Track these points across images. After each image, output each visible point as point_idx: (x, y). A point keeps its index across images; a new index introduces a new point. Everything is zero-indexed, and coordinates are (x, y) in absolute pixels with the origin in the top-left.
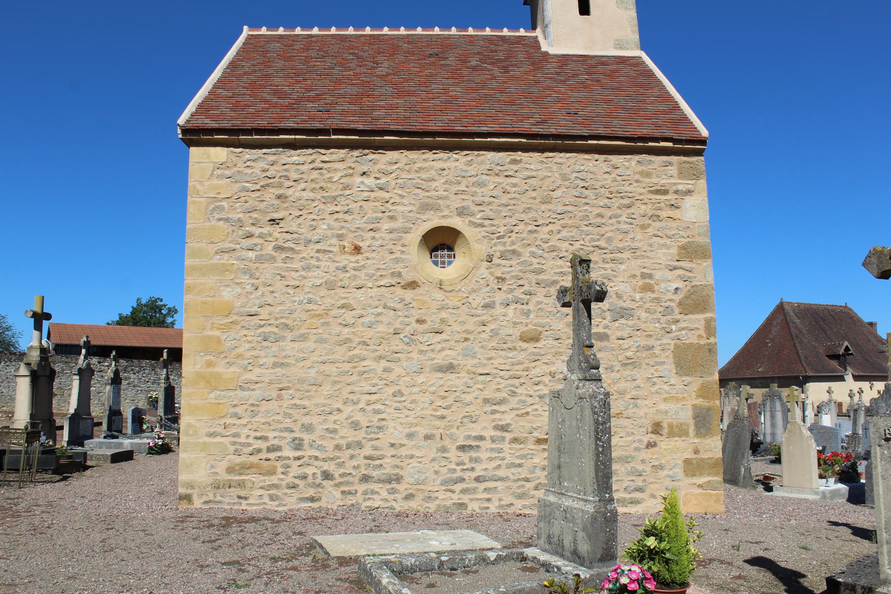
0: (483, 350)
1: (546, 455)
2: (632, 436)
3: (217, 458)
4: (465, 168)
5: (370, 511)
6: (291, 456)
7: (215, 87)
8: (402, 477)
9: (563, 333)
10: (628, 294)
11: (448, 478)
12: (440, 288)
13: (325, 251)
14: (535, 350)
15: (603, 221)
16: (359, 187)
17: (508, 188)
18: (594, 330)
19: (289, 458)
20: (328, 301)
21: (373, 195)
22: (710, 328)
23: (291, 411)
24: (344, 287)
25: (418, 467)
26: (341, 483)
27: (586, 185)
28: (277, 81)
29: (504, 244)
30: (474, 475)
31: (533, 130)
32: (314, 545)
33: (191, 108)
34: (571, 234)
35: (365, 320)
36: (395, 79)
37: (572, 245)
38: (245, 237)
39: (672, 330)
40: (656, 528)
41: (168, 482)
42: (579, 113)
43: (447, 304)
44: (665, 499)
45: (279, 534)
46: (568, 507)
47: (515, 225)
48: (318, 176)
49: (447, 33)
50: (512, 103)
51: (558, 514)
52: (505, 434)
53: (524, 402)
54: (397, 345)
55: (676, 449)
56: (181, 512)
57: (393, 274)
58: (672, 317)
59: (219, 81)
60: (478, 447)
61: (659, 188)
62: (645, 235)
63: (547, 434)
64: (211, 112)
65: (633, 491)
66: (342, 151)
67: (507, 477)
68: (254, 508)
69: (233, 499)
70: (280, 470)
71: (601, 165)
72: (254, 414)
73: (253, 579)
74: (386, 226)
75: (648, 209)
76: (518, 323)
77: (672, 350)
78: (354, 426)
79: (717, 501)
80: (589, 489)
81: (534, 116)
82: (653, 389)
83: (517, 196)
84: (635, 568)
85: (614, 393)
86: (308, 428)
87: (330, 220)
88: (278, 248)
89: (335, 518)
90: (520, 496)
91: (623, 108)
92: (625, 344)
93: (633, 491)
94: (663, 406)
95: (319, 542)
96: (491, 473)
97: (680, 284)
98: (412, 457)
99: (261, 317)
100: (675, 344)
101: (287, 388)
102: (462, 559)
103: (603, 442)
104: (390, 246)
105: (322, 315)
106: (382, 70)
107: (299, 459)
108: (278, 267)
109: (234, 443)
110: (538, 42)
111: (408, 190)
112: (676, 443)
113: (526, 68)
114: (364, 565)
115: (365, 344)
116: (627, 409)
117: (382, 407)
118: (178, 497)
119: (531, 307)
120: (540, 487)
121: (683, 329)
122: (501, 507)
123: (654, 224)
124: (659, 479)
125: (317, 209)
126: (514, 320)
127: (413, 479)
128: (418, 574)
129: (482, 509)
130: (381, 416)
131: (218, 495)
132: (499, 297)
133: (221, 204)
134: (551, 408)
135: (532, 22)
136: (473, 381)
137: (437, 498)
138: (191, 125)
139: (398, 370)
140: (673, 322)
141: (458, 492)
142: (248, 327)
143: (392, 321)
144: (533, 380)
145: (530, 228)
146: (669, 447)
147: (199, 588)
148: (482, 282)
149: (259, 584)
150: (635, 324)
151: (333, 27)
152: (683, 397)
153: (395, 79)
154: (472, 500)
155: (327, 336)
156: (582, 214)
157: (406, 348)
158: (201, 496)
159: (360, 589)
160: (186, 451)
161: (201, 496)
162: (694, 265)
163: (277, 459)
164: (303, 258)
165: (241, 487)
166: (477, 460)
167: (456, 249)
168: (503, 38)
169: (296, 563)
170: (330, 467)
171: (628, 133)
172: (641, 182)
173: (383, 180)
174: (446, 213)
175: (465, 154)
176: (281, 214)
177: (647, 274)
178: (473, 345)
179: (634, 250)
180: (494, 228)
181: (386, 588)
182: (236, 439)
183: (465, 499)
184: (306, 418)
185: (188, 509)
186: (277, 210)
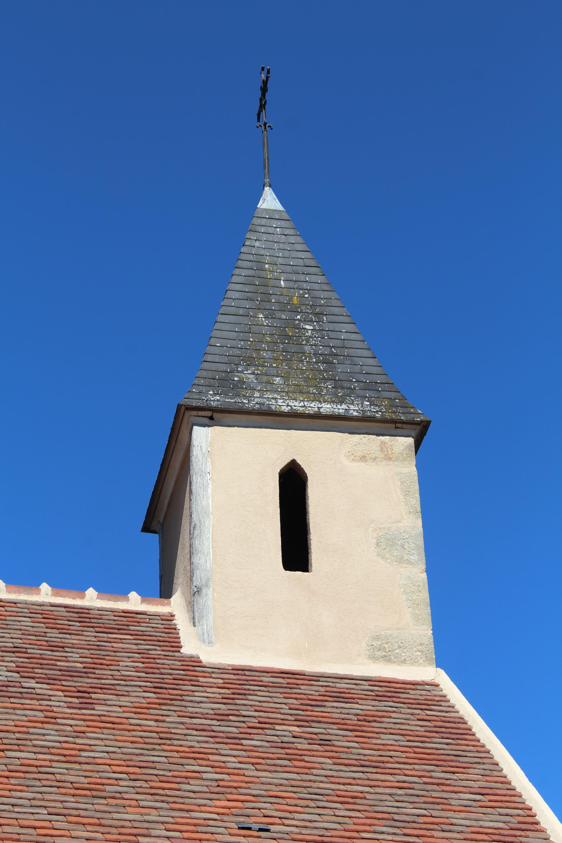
42: (272, 828)
135: (161, 577)
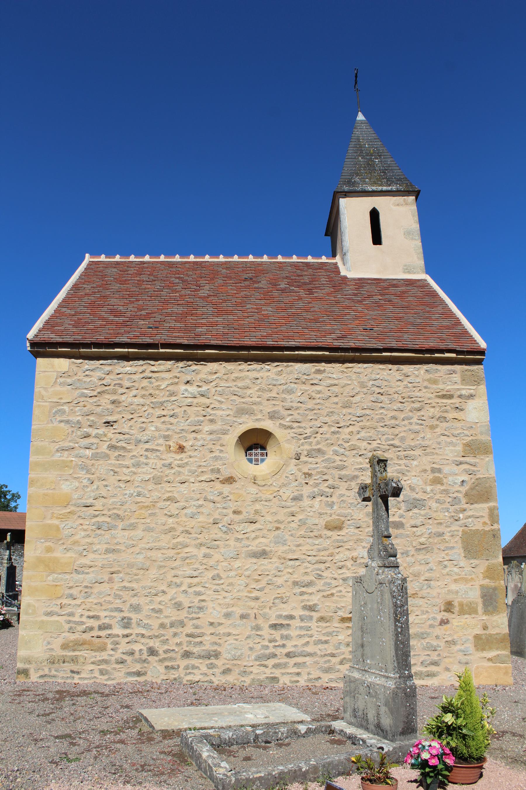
0: (292, 538)
1: (350, 632)
2: (427, 614)
3: (53, 636)
4: (276, 377)
5: (191, 684)
6: (120, 634)
7: (60, 306)
8: (220, 653)
9: (363, 522)
10: (420, 487)
11: (261, 654)
12: (255, 483)
13: (153, 450)
14: (338, 538)
15: (397, 423)
16: (183, 394)
17: (314, 394)
18: (391, 519)
19: (118, 636)
20: (156, 494)
21: (195, 401)
22: (493, 516)
23: (121, 593)
24: (169, 482)
25: (235, 643)
26: (165, 659)
27: (381, 391)
28: (113, 301)
29: (310, 444)
30: (285, 651)
31: (334, 344)
32: (139, 719)
33: (39, 324)
34: (368, 434)
35: (188, 511)
36: (215, 300)
37: (370, 444)
38: (83, 437)
39: (459, 518)
40: (452, 706)
41: (7, 656)
43: (261, 497)
44: (459, 677)
45: (108, 707)
46: (371, 683)
47: (320, 427)
48: (148, 384)
49: (259, 260)
50: (316, 320)
51: (362, 690)
52: (313, 614)
53: (329, 584)
54: (216, 534)
55: (466, 626)
56: (19, 686)
57: (212, 471)
58: (459, 507)
59: (64, 301)
60: (288, 625)
61: (445, 393)
62: (434, 434)
63: (351, 613)
64: (56, 328)
65: (429, 664)
66: (169, 363)
67: (315, 653)
68: (86, 682)
69: (66, 673)
70: (110, 646)
71: (394, 374)
72: (88, 595)
73: (83, 753)
74: (207, 428)
75: (436, 412)
76: (323, 514)
77: (460, 536)
78: (177, 606)
79: (506, 673)
80: (390, 667)
81: (336, 332)
82: (445, 571)
83: (322, 401)
84: (435, 744)
85: (410, 575)
86: (136, 608)
87: (158, 423)
88: (112, 447)
89: (159, 691)
90: (327, 670)
91: (413, 324)
92: (419, 531)
93: (429, 664)
94: (454, 587)
95: (145, 715)
96: (300, 650)
97: (466, 477)
98: (229, 634)
99: (95, 508)
100: (463, 531)
101: (118, 572)
102: (276, 733)
103: (401, 623)
104: (210, 446)
105: (150, 506)
106: (203, 293)
107: (127, 636)
108: (111, 464)
109: (69, 622)
110: (337, 268)
111: (226, 397)
112: (466, 620)
113: (328, 290)
114: (186, 739)
115: (187, 532)
116: (421, 589)
117: (202, 589)
118: (16, 671)
119: (334, 499)
120: (344, 661)
121: (470, 517)
122: (310, 680)
123: (441, 424)
124: (453, 653)
125: (146, 413)
126: (320, 511)
127: (230, 655)
128: (235, 747)
129: (293, 682)
130: (202, 598)
131: (53, 670)
132: (306, 491)
133: (62, 408)
134: (354, 592)
136: (284, 565)
137: (252, 672)
138: (38, 339)
139: (217, 556)
140: (460, 511)
141: (270, 666)
142: (84, 516)
143: (211, 512)
144: (337, 564)
145: (333, 429)
146: (460, 623)
147: (33, 763)
148: (291, 477)
149: (89, 757)
150: (427, 513)
151: (162, 255)
152: (472, 578)
153: (215, 300)
154: (283, 674)
155: (154, 525)
156: (378, 417)
157: (224, 536)
158: (37, 670)
159: (181, 762)
160: (25, 629)
161: (37, 670)
162: (477, 460)
163: (107, 636)
164: (134, 456)
165: (74, 662)
166: (287, 637)
167: (268, 448)
168: (307, 264)
169: (123, 736)
170: (155, 644)
171: (417, 346)
172: (429, 388)
173: (204, 388)
174: (259, 417)
175: (276, 365)
176: (115, 417)
177: (437, 469)
178: (283, 533)
179: (424, 448)
180: (301, 430)
181: (206, 761)
182: (71, 618)
183: (277, 673)
184: (134, 599)
185: (25, 683)
186: (112, 413)
